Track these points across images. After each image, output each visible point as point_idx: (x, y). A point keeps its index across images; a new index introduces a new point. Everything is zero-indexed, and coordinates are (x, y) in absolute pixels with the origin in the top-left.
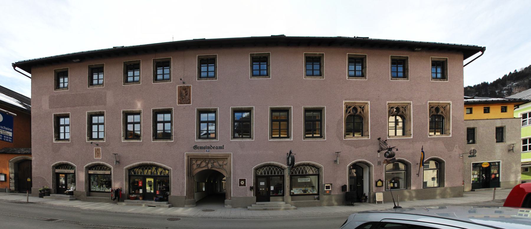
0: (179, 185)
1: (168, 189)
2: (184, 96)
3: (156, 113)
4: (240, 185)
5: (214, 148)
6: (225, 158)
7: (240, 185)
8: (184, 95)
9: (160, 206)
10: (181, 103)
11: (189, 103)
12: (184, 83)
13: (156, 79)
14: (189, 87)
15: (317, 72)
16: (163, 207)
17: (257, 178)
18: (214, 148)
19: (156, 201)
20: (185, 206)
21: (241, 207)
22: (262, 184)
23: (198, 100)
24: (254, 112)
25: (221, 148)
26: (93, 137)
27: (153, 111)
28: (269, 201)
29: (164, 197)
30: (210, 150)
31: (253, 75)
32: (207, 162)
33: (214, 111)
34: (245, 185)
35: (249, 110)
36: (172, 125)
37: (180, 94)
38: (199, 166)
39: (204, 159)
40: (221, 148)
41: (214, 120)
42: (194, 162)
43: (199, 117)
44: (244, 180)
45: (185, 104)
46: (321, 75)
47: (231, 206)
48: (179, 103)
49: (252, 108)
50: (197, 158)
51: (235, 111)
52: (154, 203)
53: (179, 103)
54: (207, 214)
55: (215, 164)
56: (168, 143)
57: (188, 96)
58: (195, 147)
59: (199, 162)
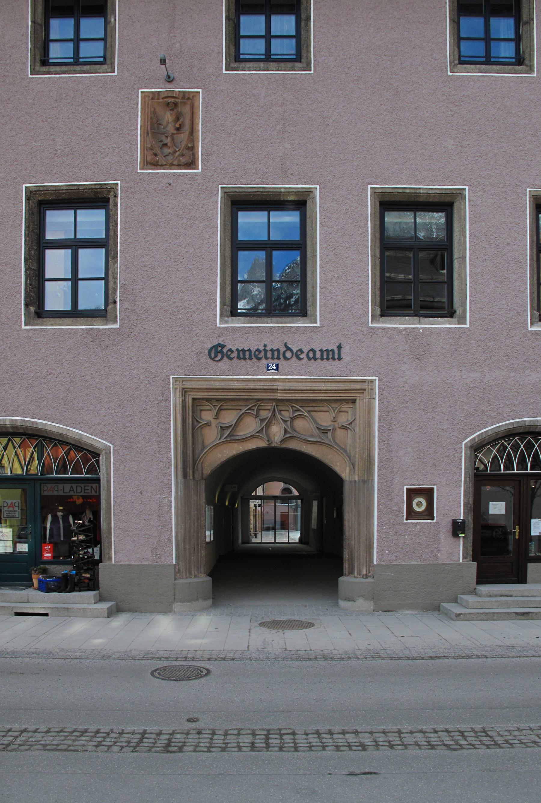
0: (147, 514)
1: (95, 534)
2: (170, 131)
3: (43, 203)
4: (411, 514)
5: (298, 355)
6: (346, 398)
7: (411, 514)
8: (171, 129)
9: (67, 612)
10: (155, 165)
11: (191, 164)
12: (169, 80)
13: (43, 60)
14: (189, 99)
15: (506, 50)
16: (83, 614)
17: (481, 483)
18: (298, 355)
19: (45, 587)
20: (177, 606)
21: (410, 607)
22: (497, 508)
23: (230, 155)
24: (466, 210)
25: (332, 355)
26: (50, 305)
27: (31, 194)
28: (521, 579)
29: (78, 569)
30: (282, 363)
31: (462, 61)
32: (265, 414)
33: (300, 204)
34: (429, 513)
35: (445, 204)
36: (110, 257)
37: (153, 128)
38: (230, 433)
39: (252, 402)
40: (332, 355)
41: (297, 237)
42: (207, 416)
43: (233, 226)
44: (428, 494)
45: (171, 166)
46: (520, 60)
47: (369, 605)
48: (147, 163)
49: (460, 193)
50: (222, 400)
51: (388, 203)
52: (34, 598)
53: (147, 163)
54: (295, 640)
55: (299, 424)
56: (97, 335)
57: (183, 137)
58: (218, 352)
59: (229, 417)
